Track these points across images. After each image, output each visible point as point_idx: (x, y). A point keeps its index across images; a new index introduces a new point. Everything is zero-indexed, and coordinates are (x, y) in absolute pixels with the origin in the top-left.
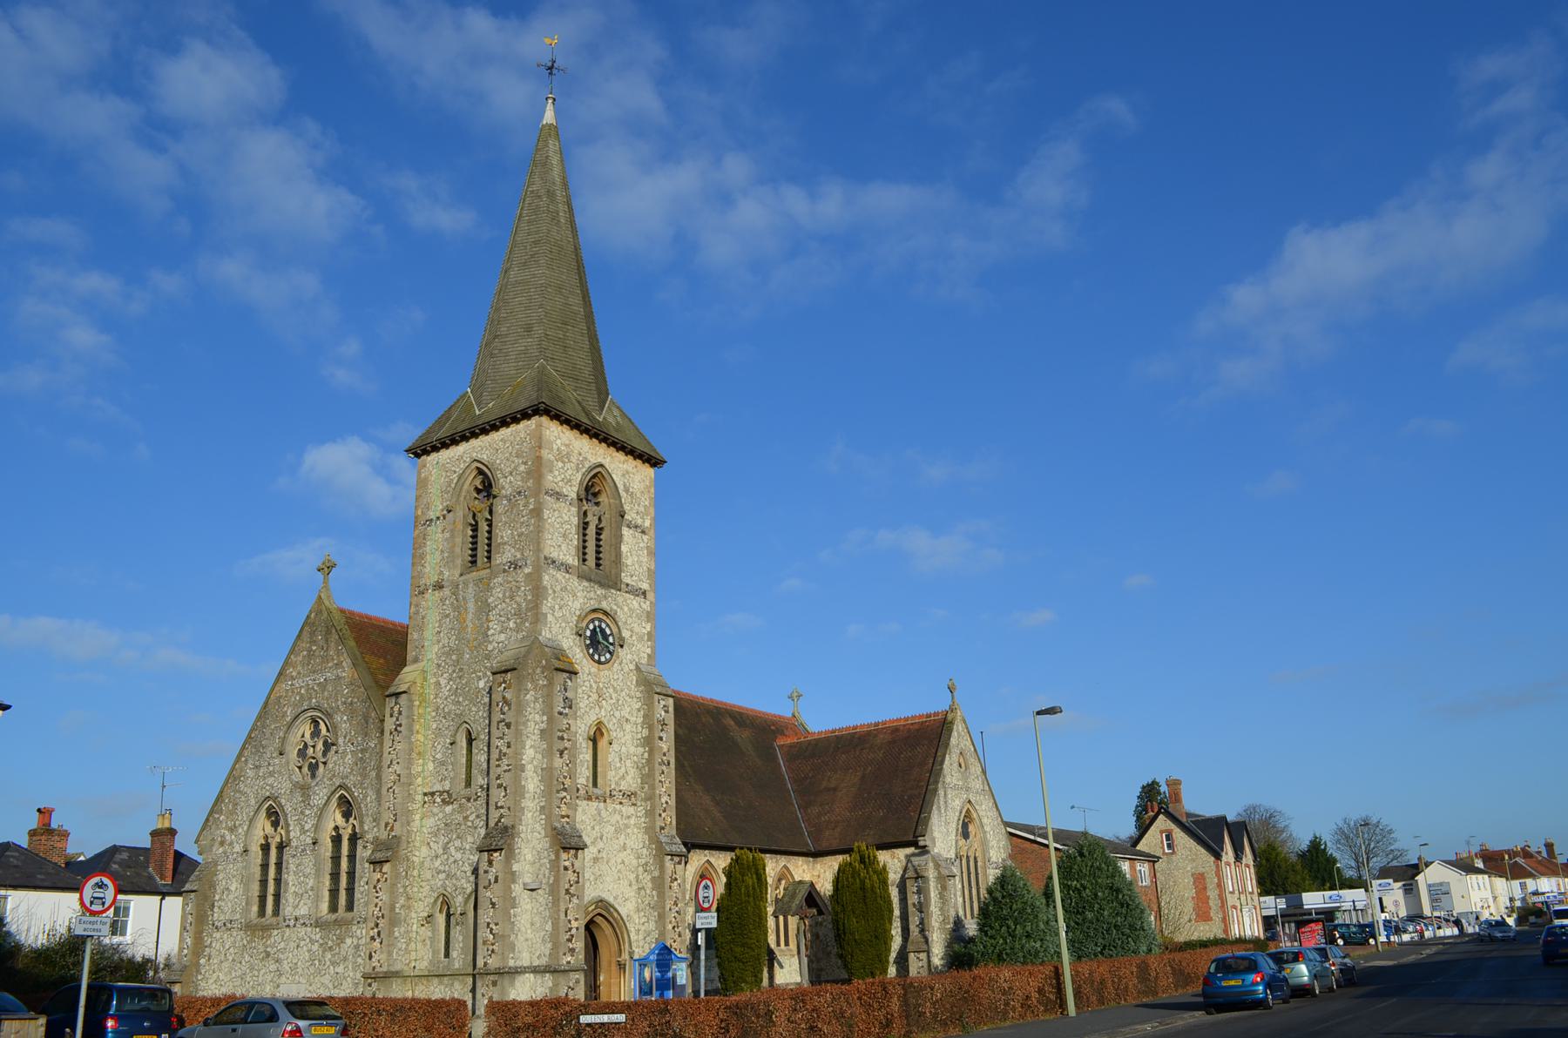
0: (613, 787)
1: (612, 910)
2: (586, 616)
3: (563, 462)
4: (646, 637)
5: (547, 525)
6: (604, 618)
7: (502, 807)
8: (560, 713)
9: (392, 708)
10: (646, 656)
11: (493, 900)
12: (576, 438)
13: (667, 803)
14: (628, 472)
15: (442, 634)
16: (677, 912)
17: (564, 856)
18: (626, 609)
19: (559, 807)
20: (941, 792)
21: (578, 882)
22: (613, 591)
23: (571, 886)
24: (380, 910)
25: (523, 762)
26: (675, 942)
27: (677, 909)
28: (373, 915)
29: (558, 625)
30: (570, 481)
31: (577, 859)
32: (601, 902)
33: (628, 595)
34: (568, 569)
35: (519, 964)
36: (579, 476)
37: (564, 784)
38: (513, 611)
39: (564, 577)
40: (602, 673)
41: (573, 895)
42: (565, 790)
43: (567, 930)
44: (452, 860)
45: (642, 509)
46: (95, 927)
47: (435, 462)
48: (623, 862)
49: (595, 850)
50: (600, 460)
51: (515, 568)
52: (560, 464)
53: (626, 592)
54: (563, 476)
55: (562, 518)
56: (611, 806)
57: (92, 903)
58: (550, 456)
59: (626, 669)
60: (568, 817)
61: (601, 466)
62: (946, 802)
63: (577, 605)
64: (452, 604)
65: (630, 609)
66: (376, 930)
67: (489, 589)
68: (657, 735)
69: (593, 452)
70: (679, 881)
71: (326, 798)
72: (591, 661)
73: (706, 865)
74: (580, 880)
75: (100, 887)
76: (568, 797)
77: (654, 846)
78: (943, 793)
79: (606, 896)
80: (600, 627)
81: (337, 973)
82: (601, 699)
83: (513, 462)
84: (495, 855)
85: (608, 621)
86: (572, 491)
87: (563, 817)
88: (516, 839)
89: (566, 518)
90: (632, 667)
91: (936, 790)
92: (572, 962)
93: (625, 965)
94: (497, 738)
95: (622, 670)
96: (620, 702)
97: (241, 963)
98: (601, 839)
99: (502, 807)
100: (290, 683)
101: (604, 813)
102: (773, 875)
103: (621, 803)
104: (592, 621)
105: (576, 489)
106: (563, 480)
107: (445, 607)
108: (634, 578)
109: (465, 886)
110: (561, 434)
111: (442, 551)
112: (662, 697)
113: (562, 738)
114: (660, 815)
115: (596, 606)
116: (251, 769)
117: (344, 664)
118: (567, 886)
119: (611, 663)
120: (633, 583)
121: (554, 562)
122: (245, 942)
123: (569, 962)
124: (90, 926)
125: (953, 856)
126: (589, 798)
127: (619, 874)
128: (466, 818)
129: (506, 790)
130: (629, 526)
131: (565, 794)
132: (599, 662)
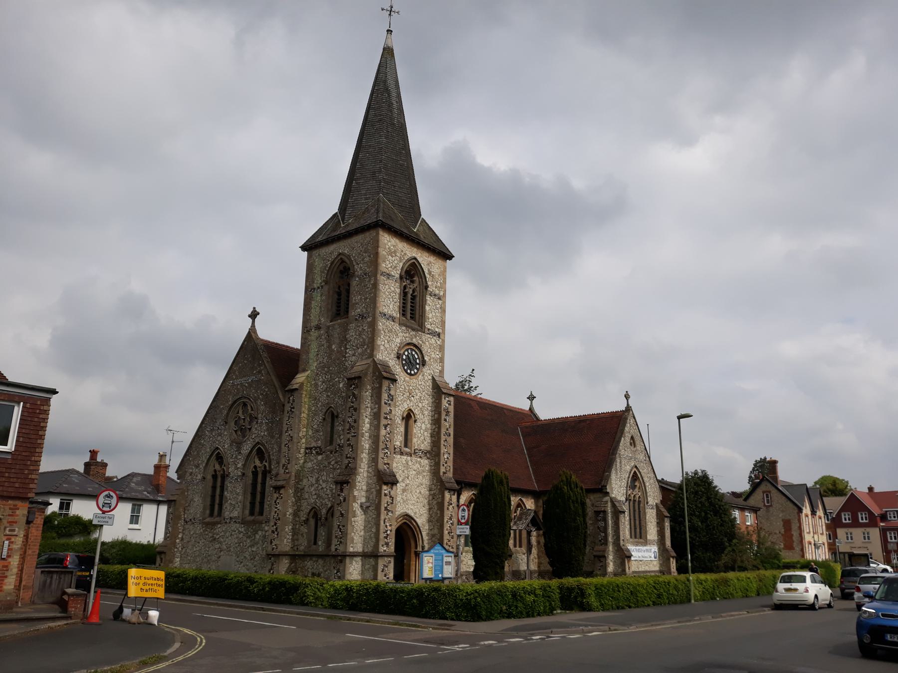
0: (416, 448)
1: (413, 521)
2: (403, 347)
3: (392, 257)
6: (414, 348)
7: (350, 458)
8: (386, 403)
9: (289, 398)
11: (342, 512)
13: (448, 458)
14: (430, 263)
15: (319, 356)
16: (451, 523)
17: (385, 487)
20: (618, 460)
21: (392, 503)
22: (420, 333)
23: (388, 505)
24: (278, 516)
25: (363, 431)
26: (449, 541)
27: (451, 522)
28: (274, 518)
29: (386, 352)
30: (395, 267)
31: (392, 489)
32: (407, 516)
35: (356, 550)
36: (401, 264)
37: (386, 445)
38: (360, 343)
40: (412, 381)
42: (387, 448)
44: (320, 487)
46: (105, 520)
47: (317, 255)
48: (420, 493)
49: (404, 485)
51: (362, 318)
52: (390, 257)
53: (428, 334)
54: (391, 264)
55: (390, 289)
56: (414, 458)
57: (103, 506)
58: (384, 252)
61: (415, 259)
62: (621, 466)
63: (398, 340)
64: (326, 338)
66: (275, 527)
67: (346, 330)
68: (443, 418)
70: (453, 505)
71: (250, 449)
74: (394, 502)
75: (108, 497)
76: (389, 453)
77: (439, 484)
81: (253, 551)
82: (411, 396)
83: (362, 255)
84: (344, 485)
85: (416, 350)
86: (396, 274)
87: (385, 464)
90: (430, 378)
91: (615, 459)
92: (387, 550)
94: (349, 417)
96: (422, 398)
97: (199, 543)
98: (408, 478)
99: (350, 458)
100: (231, 382)
101: (410, 463)
103: (420, 457)
104: (407, 350)
105: (399, 272)
106: (391, 267)
107: (321, 340)
108: (433, 325)
109: (327, 503)
111: (320, 307)
113: (386, 418)
114: (443, 465)
115: (410, 341)
116: (208, 431)
117: (263, 372)
118: (386, 505)
121: (385, 315)
122: (202, 531)
123: (385, 551)
125: (624, 499)
126: (402, 454)
127: (417, 499)
128: (329, 463)
129: (352, 448)
130: (430, 295)
131: (387, 451)
132: (410, 374)
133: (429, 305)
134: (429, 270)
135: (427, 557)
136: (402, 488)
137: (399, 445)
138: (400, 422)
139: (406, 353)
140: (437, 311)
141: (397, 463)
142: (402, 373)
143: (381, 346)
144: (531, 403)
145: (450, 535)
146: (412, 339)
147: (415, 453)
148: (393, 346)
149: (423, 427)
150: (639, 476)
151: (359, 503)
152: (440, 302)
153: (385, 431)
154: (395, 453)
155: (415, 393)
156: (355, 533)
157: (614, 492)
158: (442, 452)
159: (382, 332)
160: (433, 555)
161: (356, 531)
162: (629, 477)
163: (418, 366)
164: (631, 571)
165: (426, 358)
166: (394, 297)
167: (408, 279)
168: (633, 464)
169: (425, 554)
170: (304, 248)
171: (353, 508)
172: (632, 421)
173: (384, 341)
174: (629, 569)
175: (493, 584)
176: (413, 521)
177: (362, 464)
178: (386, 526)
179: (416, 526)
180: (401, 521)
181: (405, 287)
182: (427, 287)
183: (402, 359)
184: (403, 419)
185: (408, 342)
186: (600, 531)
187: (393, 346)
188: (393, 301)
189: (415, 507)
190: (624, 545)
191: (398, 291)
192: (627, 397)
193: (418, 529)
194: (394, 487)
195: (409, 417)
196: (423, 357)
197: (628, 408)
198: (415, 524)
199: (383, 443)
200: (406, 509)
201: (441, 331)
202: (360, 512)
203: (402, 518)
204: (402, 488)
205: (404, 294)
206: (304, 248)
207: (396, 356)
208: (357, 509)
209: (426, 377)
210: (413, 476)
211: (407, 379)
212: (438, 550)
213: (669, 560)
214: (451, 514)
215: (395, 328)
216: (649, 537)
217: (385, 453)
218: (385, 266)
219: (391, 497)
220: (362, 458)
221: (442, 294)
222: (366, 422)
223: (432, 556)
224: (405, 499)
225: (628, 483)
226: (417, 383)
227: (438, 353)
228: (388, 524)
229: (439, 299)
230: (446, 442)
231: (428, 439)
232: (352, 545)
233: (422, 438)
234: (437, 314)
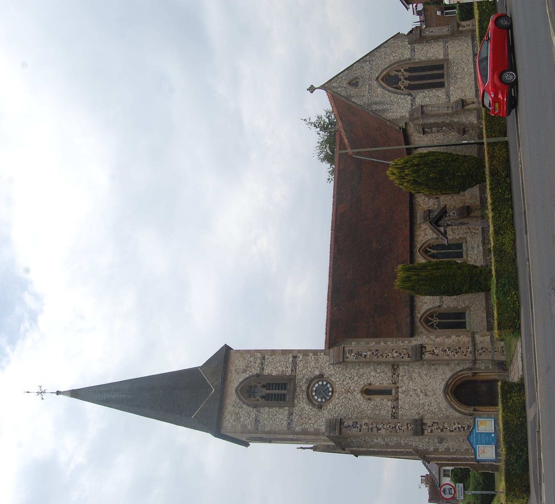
0: (391, 382)
1: (449, 383)
3: (240, 417)
4: (316, 356)
5: (272, 429)
6: (311, 388)
8: (360, 431)
10: (325, 357)
12: (227, 408)
13: (396, 352)
14: (236, 370)
16: (449, 351)
17: (426, 432)
18: (304, 372)
19: (404, 430)
20: (375, 107)
22: (296, 381)
23: (439, 428)
25: (384, 444)
26: (463, 352)
27: (447, 350)
29: (319, 421)
31: (427, 424)
33: (297, 370)
34: (291, 414)
36: (245, 406)
39: (295, 417)
41: (444, 426)
42: (395, 427)
43: (459, 430)
45: (252, 359)
46: (460, 490)
48: (426, 375)
50: (234, 391)
52: (241, 420)
53: (296, 371)
54: (247, 418)
56: (400, 384)
57: (451, 494)
58: (239, 427)
59: (333, 372)
60: (408, 424)
65: (304, 369)
69: (232, 398)
70: (434, 349)
72: (333, 397)
73: (421, 251)
74: (436, 421)
75: (445, 491)
76: (399, 424)
78: (374, 106)
79: (442, 387)
80: (315, 391)
82: (350, 391)
86: (253, 412)
88: (419, 448)
89: (266, 416)
93: (474, 373)
95: (334, 374)
96: (350, 376)
101: (404, 388)
102: (424, 197)
103: (398, 376)
105: (252, 409)
106: (249, 418)
108: (288, 365)
110: (226, 419)
112: (344, 356)
113: (372, 428)
115: (305, 393)
119: (332, 383)
120: (291, 366)
121: (289, 423)
124: (460, 493)
125: (409, 97)
126: (397, 399)
127: (432, 378)
130: (263, 369)
131: (397, 426)
132: (332, 392)
133: (272, 370)
134: (243, 372)
135: (480, 454)
136: (424, 397)
137: (391, 402)
138: (372, 403)
139: (316, 397)
140: (275, 360)
141: (405, 404)
142: (333, 402)
143: (315, 427)
144: (317, 88)
145: (458, 352)
146: (303, 391)
147: (395, 383)
148: (312, 413)
149: (373, 374)
150: (385, 73)
151: (439, 445)
152: (267, 357)
153: (382, 430)
154: (398, 407)
155: (347, 386)
156: (461, 448)
157: (404, 114)
158: (392, 359)
159: (303, 427)
160: (478, 446)
161: (459, 446)
162: (389, 91)
163: (325, 383)
164: (475, 100)
165: (317, 373)
166: (273, 414)
167: (254, 390)
168: (376, 83)
169: (478, 458)
171: (443, 451)
172: (335, 84)
173: (310, 423)
174: (473, 103)
175: (485, 146)
176: (449, 383)
177: (409, 444)
178: (455, 429)
179: (453, 378)
180: (449, 397)
182: (258, 375)
183: (322, 402)
184: (369, 399)
185: (307, 397)
186: (441, 130)
187: (312, 413)
188: (276, 415)
189: (438, 380)
190: (452, 107)
191: (267, 409)
192: (312, 89)
193: (455, 381)
194: (425, 421)
195: (368, 392)
196: (316, 377)
197: (323, 87)
198: (451, 380)
199: (391, 432)
200: (440, 390)
201: (291, 355)
202: (445, 443)
203: (448, 396)
204: (424, 397)
207: (320, 410)
208: (444, 447)
209: (332, 371)
210: (414, 385)
211: (336, 396)
212: (473, 438)
213: (461, 32)
214: (442, 351)
215: (298, 412)
216: (441, 57)
217: (400, 429)
218: (249, 426)
219: (433, 425)
220: (405, 443)
221: (259, 355)
222: (377, 441)
223: (478, 421)
224: (432, 393)
225: (394, 93)
226: (338, 383)
227: (310, 358)
228: (454, 427)
229: (264, 358)
230: (383, 355)
231: (382, 367)
232: (470, 450)
233: (382, 374)
234: (278, 360)
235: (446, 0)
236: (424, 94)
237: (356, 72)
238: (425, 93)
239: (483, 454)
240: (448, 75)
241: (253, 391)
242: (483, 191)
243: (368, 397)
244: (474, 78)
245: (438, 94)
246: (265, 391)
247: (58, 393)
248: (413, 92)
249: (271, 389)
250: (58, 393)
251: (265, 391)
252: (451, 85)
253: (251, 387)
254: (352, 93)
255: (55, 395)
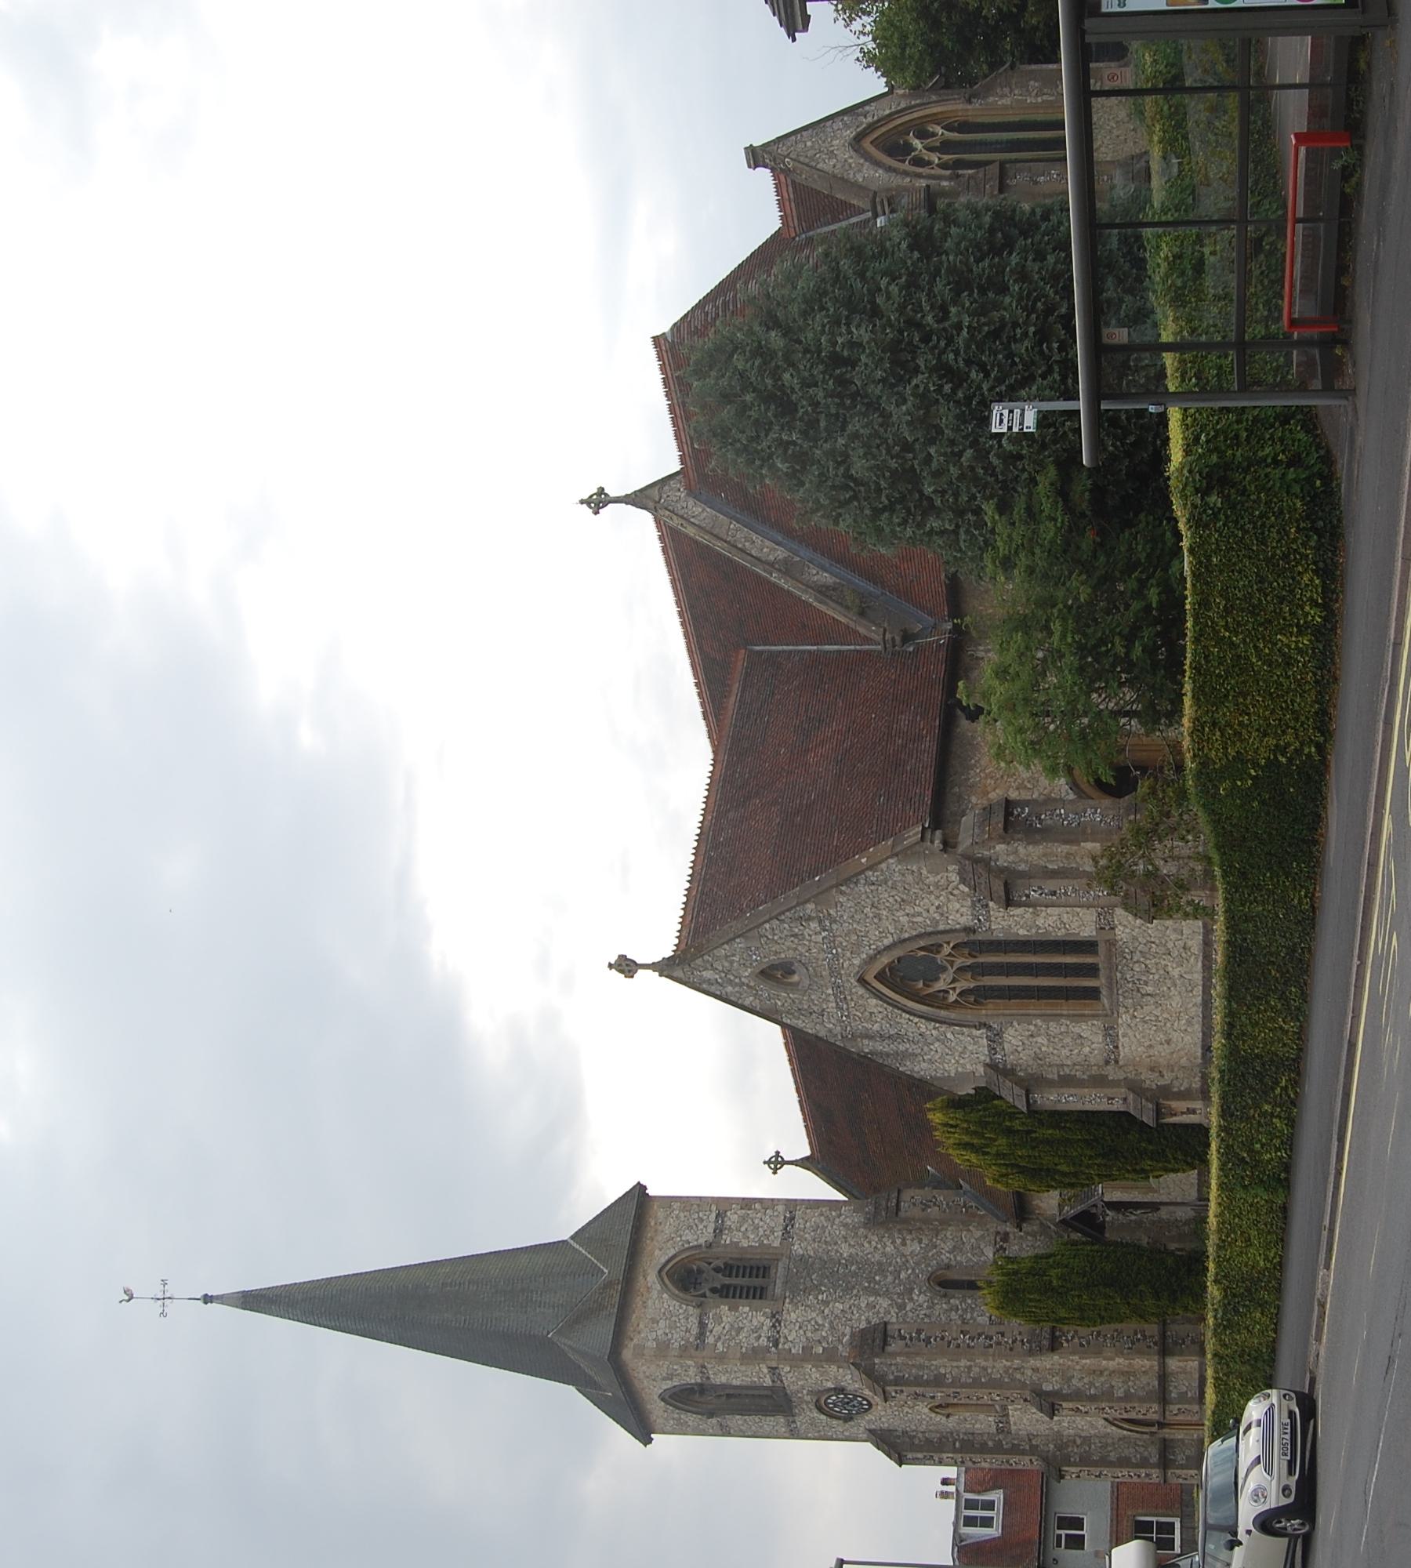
20: (867, 1046)
69: (649, 1279)
78: (866, 1042)
167: (696, 1279)
170: (646, 1440)
181: (714, 1290)
184: (945, 1296)
192: (598, 501)
195: (946, 1283)
205: (725, 1293)
206: (646, 1440)
235: (1109, 2)
236: (1032, 1028)
237: (775, 948)
238: (1035, 1025)
239: (1166, 1045)
240: (1111, 984)
241: (694, 1280)
242: (1203, 1183)
243: (943, 1291)
244: (1200, 998)
245: (1077, 1030)
246: (721, 1280)
247: (207, 1299)
248: (989, 1011)
249: (731, 1295)
250: (207, 1299)
251: (721, 1280)
252: (1122, 1010)
253: (690, 1272)
254: (779, 1003)
255: (200, 1303)
